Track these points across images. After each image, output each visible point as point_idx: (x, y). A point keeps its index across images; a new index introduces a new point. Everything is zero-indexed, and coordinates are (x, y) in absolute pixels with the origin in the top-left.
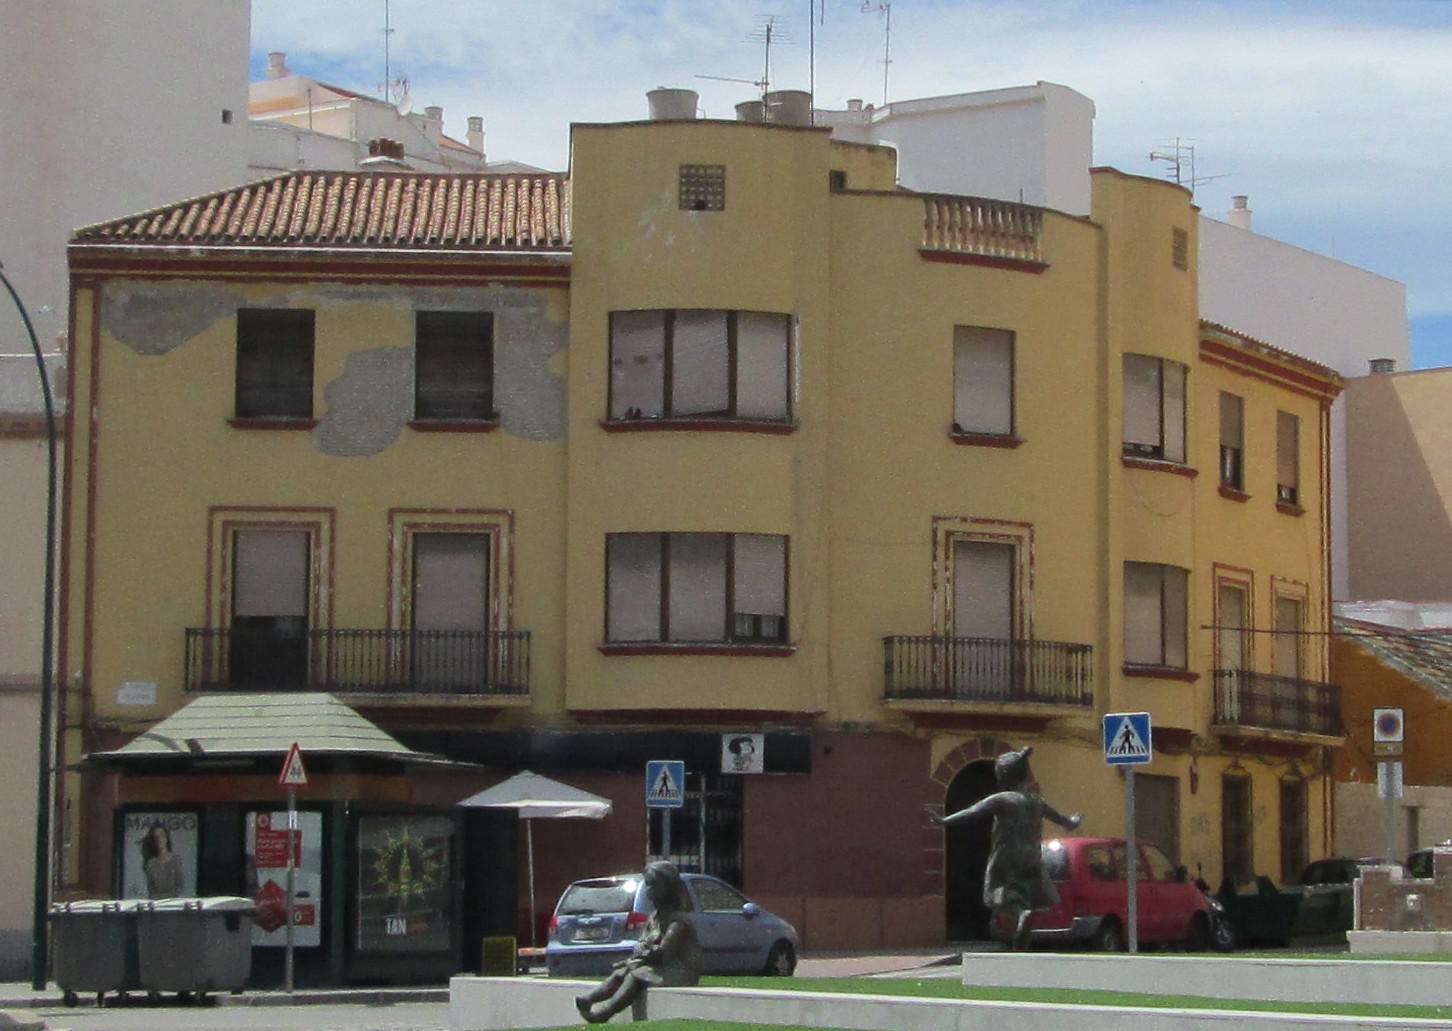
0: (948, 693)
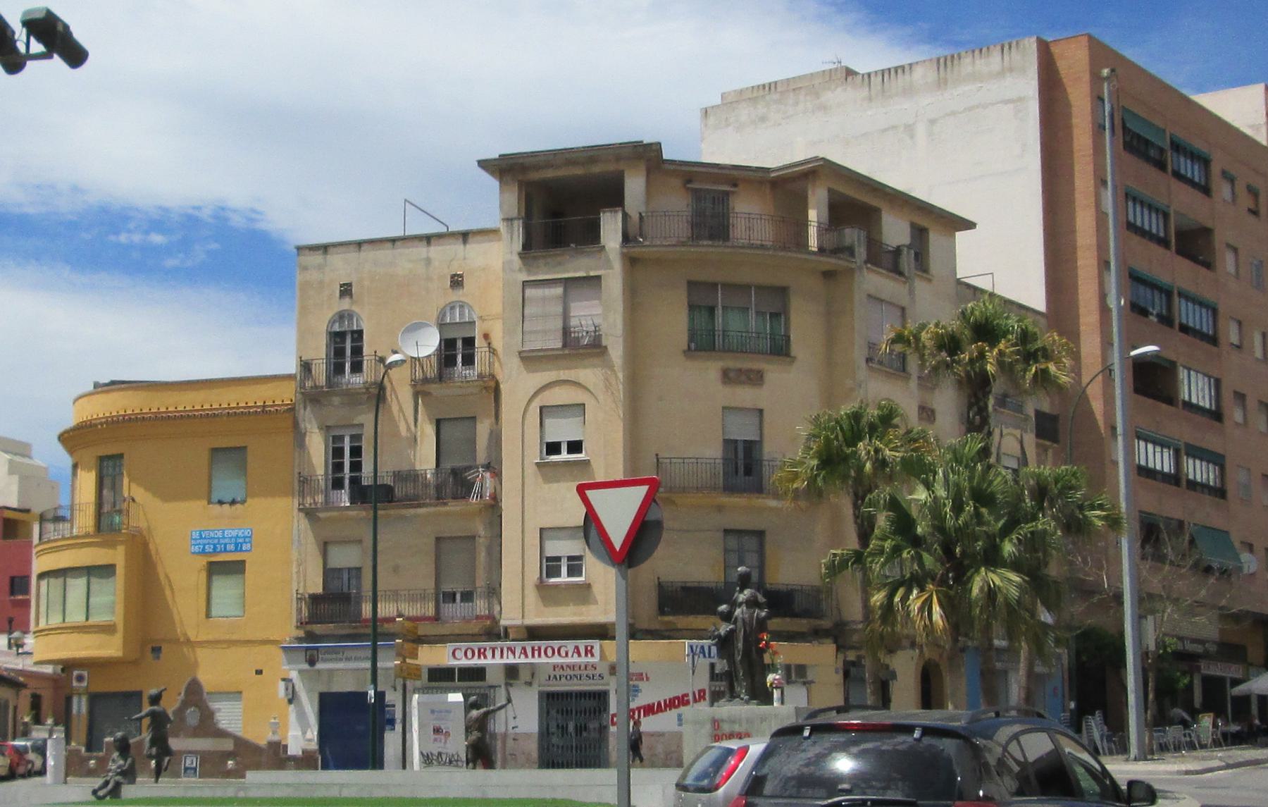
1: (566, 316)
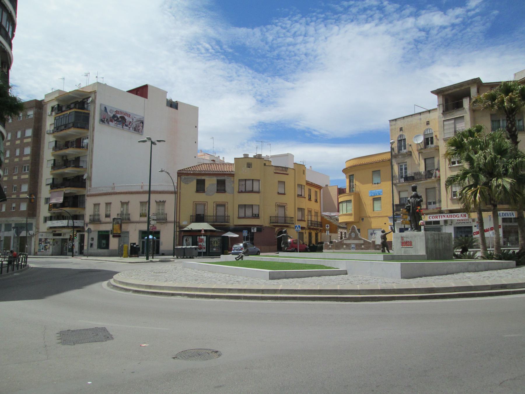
0: (277, 223)
1: (455, 128)
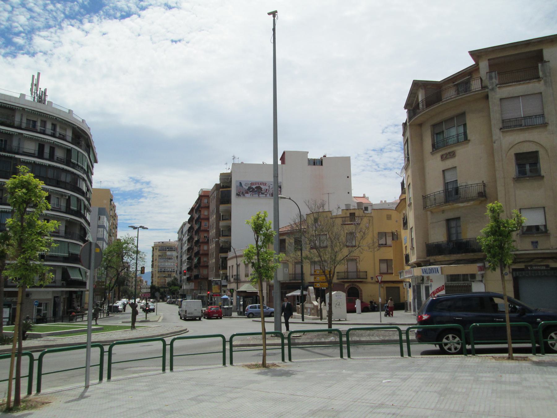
0: (348, 278)
